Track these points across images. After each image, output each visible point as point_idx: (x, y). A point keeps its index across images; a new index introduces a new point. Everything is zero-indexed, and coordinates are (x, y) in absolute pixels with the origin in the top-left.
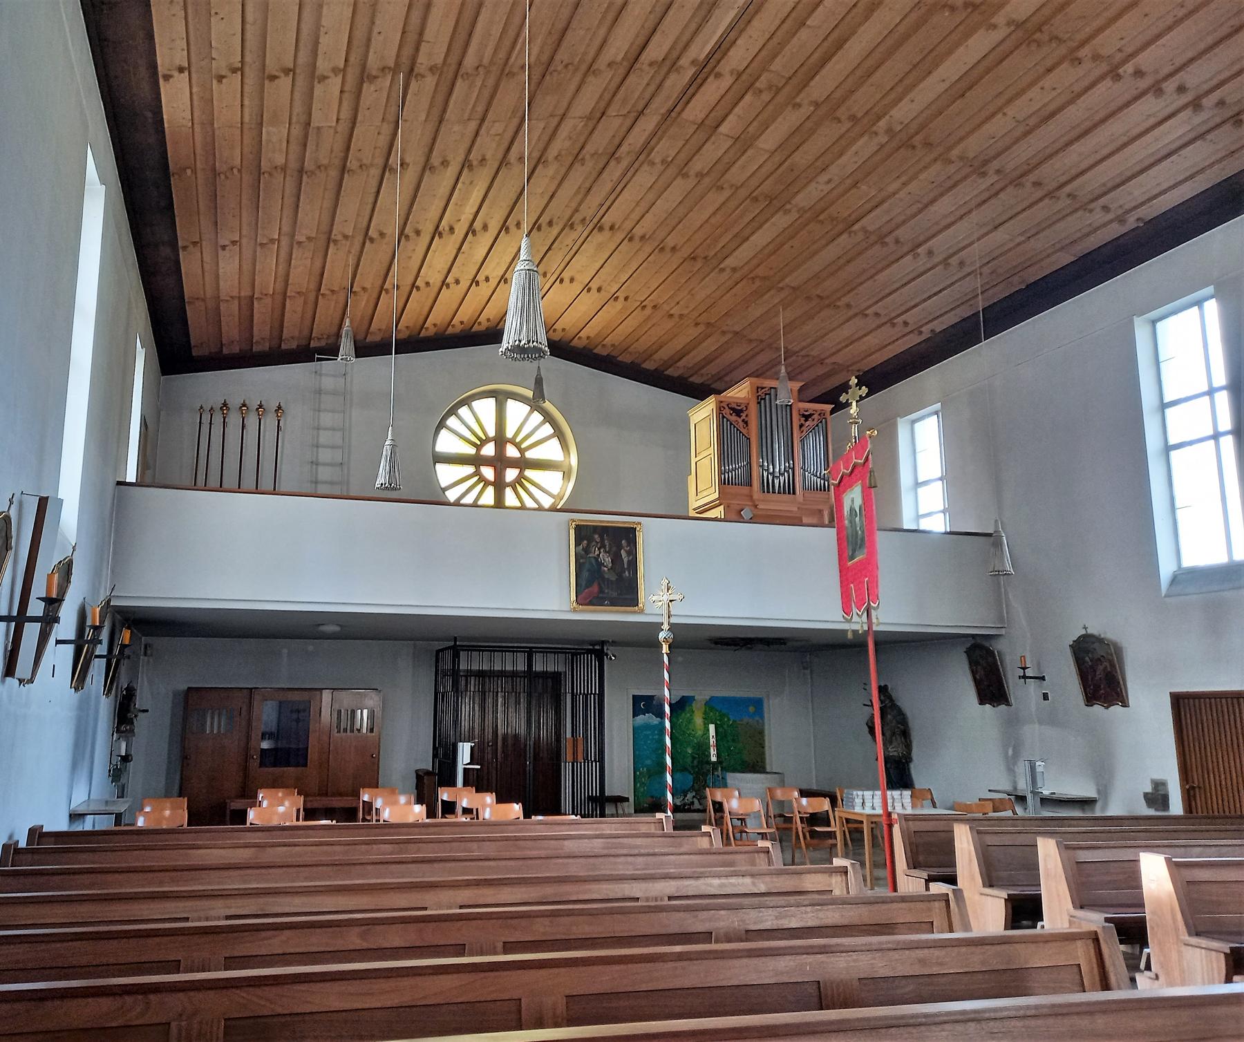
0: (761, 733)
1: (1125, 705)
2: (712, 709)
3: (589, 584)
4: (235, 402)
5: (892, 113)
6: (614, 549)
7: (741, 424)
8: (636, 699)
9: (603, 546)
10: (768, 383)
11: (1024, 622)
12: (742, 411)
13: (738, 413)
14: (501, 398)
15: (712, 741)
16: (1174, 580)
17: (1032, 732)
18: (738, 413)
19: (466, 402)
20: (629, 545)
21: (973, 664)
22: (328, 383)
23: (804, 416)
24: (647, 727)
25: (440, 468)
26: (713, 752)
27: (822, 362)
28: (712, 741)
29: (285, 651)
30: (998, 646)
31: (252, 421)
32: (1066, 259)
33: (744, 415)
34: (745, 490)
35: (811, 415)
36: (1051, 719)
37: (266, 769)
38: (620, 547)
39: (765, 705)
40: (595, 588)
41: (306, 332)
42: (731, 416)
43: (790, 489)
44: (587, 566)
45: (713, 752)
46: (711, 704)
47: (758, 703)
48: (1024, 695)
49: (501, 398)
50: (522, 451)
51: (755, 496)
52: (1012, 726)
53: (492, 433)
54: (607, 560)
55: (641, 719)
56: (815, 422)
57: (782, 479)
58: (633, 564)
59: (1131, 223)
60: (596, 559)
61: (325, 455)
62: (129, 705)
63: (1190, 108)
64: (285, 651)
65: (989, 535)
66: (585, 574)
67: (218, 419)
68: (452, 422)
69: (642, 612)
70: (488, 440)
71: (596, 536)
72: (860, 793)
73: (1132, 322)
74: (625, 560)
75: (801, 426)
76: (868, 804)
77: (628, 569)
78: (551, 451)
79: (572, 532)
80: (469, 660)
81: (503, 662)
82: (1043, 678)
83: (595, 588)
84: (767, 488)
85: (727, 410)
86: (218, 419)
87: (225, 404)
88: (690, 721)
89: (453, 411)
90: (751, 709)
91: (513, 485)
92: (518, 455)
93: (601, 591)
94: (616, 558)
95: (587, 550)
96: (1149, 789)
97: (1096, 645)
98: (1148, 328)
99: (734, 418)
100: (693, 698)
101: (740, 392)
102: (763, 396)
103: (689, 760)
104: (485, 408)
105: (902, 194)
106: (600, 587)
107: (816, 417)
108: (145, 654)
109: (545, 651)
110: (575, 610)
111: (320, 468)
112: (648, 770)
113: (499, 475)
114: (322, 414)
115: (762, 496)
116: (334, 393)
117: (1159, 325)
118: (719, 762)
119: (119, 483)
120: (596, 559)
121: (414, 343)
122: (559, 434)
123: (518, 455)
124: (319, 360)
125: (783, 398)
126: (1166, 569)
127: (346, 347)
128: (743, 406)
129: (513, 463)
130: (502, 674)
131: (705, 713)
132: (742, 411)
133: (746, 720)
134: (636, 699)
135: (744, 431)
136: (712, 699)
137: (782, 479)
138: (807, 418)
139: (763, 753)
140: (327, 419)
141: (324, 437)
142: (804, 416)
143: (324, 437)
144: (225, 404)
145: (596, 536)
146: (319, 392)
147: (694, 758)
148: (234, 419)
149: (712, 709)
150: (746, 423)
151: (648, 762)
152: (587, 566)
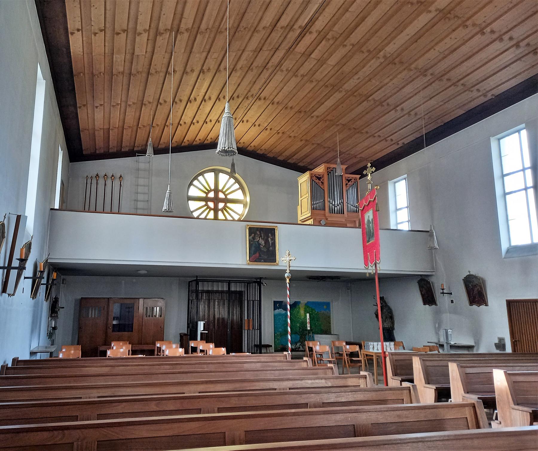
0: (329, 317)
1: (487, 305)
2: (308, 307)
3: (255, 253)
4: (102, 174)
5: (386, 49)
6: (266, 238)
7: (321, 183)
8: (275, 303)
9: (261, 236)
10: (332, 166)
11: (443, 269)
12: (321, 178)
13: (319, 179)
14: (217, 172)
15: (308, 321)
16: (508, 251)
17: (446, 317)
18: (319, 179)
19: (201, 174)
20: (272, 236)
21: (421, 288)
22: (142, 166)
23: (348, 180)
24: (280, 314)
25: (190, 202)
26: (308, 325)
27: (355, 157)
28: (308, 321)
29: (123, 282)
30: (432, 280)
31: (109, 182)
32: (461, 112)
33: (322, 180)
34: (322, 212)
35: (351, 180)
36: (455, 311)
37: (115, 333)
38: (268, 237)
39: (331, 305)
40: (257, 255)
41: (132, 144)
42: (316, 180)
43: (342, 212)
44: (254, 245)
45: (308, 325)
46: (307, 305)
47: (328, 304)
48: (443, 301)
49: (217, 172)
50: (226, 195)
51: (327, 215)
52: (438, 314)
53: (213, 187)
54: (262, 242)
55: (277, 311)
56: (353, 183)
57: (338, 207)
58: (274, 244)
59: (489, 96)
60: (258, 242)
61: (141, 197)
62: (56, 305)
63: (515, 47)
64: (123, 282)
65: (428, 232)
66: (253, 249)
67: (94, 181)
68: (195, 183)
69: (277, 265)
70: (211, 190)
71: (258, 232)
72: (372, 343)
73: (489, 139)
74: (270, 243)
75: (347, 184)
76: (375, 348)
77: (272, 246)
78: (238, 195)
79: (247, 230)
80: (203, 286)
81: (218, 286)
82: (451, 294)
83: (257, 255)
84: (332, 211)
85: (315, 178)
86: (94, 181)
87: (97, 175)
88: (298, 312)
89: (196, 178)
90: (325, 307)
91: (222, 210)
92: (224, 197)
93: (260, 256)
94: (267, 242)
95: (254, 238)
96: (497, 342)
97: (474, 279)
98: (496, 142)
99: (317, 181)
100: (299, 302)
101: (320, 170)
102: (330, 172)
103: (298, 329)
104: (210, 177)
105: (390, 84)
106: (259, 254)
107: (353, 180)
108: (63, 283)
109: (236, 282)
110: (248, 264)
111: (139, 203)
112: (280, 333)
113: (216, 206)
114: (139, 179)
115: (329, 215)
116: (145, 170)
117: (501, 141)
118: (311, 330)
119: (51, 209)
120: (258, 242)
121: (179, 149)
122: (242, 188)
123: (224, 197)
124: (138, 156)
125: (339, 172)
126: (504, 246)
127: (150, 150)
128: (321, 176)
129: (222, 200)
130: (217, 292)
131: (305, 309)
132: (321, 178)
133: (322, 311)
134: (275, 303)
135: (322, 187)
136: (308, 302)
137: (338, 207)
138: (349, 181)
139: (330, 326)
140: (141, 181)
141: (140, 189)
142: (348, 180)
143: (140, 189)
144: (97, 175)
145: (258, 232)
146: (138, 170)
147: (300, 328)
148: (101, 181)
149: (308, 307)
150: (323, 183)
151: (280, 330)
152: (254, 245)
